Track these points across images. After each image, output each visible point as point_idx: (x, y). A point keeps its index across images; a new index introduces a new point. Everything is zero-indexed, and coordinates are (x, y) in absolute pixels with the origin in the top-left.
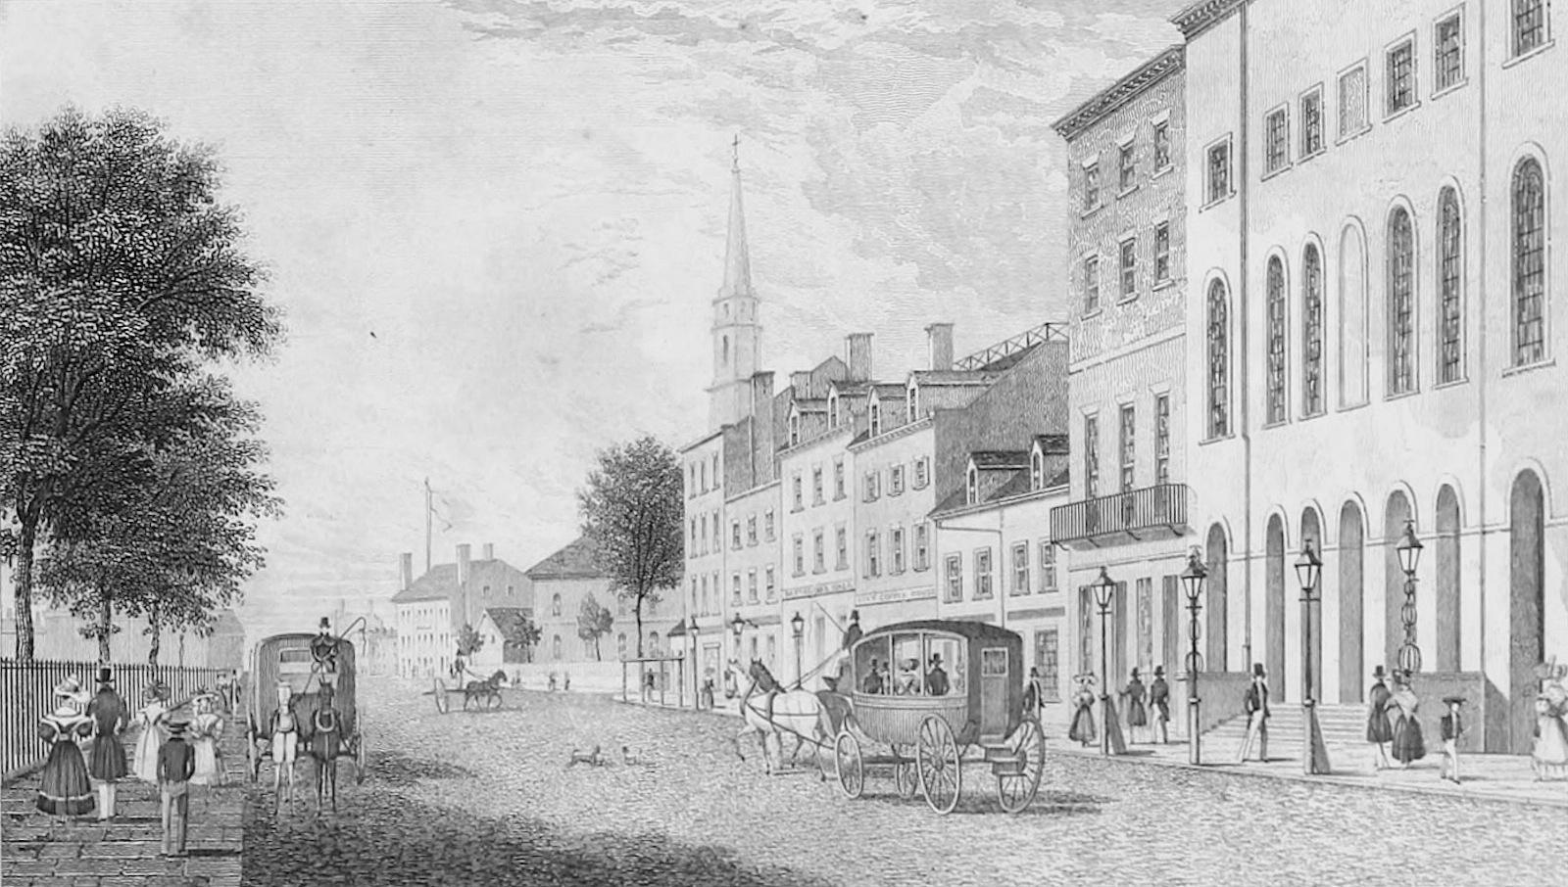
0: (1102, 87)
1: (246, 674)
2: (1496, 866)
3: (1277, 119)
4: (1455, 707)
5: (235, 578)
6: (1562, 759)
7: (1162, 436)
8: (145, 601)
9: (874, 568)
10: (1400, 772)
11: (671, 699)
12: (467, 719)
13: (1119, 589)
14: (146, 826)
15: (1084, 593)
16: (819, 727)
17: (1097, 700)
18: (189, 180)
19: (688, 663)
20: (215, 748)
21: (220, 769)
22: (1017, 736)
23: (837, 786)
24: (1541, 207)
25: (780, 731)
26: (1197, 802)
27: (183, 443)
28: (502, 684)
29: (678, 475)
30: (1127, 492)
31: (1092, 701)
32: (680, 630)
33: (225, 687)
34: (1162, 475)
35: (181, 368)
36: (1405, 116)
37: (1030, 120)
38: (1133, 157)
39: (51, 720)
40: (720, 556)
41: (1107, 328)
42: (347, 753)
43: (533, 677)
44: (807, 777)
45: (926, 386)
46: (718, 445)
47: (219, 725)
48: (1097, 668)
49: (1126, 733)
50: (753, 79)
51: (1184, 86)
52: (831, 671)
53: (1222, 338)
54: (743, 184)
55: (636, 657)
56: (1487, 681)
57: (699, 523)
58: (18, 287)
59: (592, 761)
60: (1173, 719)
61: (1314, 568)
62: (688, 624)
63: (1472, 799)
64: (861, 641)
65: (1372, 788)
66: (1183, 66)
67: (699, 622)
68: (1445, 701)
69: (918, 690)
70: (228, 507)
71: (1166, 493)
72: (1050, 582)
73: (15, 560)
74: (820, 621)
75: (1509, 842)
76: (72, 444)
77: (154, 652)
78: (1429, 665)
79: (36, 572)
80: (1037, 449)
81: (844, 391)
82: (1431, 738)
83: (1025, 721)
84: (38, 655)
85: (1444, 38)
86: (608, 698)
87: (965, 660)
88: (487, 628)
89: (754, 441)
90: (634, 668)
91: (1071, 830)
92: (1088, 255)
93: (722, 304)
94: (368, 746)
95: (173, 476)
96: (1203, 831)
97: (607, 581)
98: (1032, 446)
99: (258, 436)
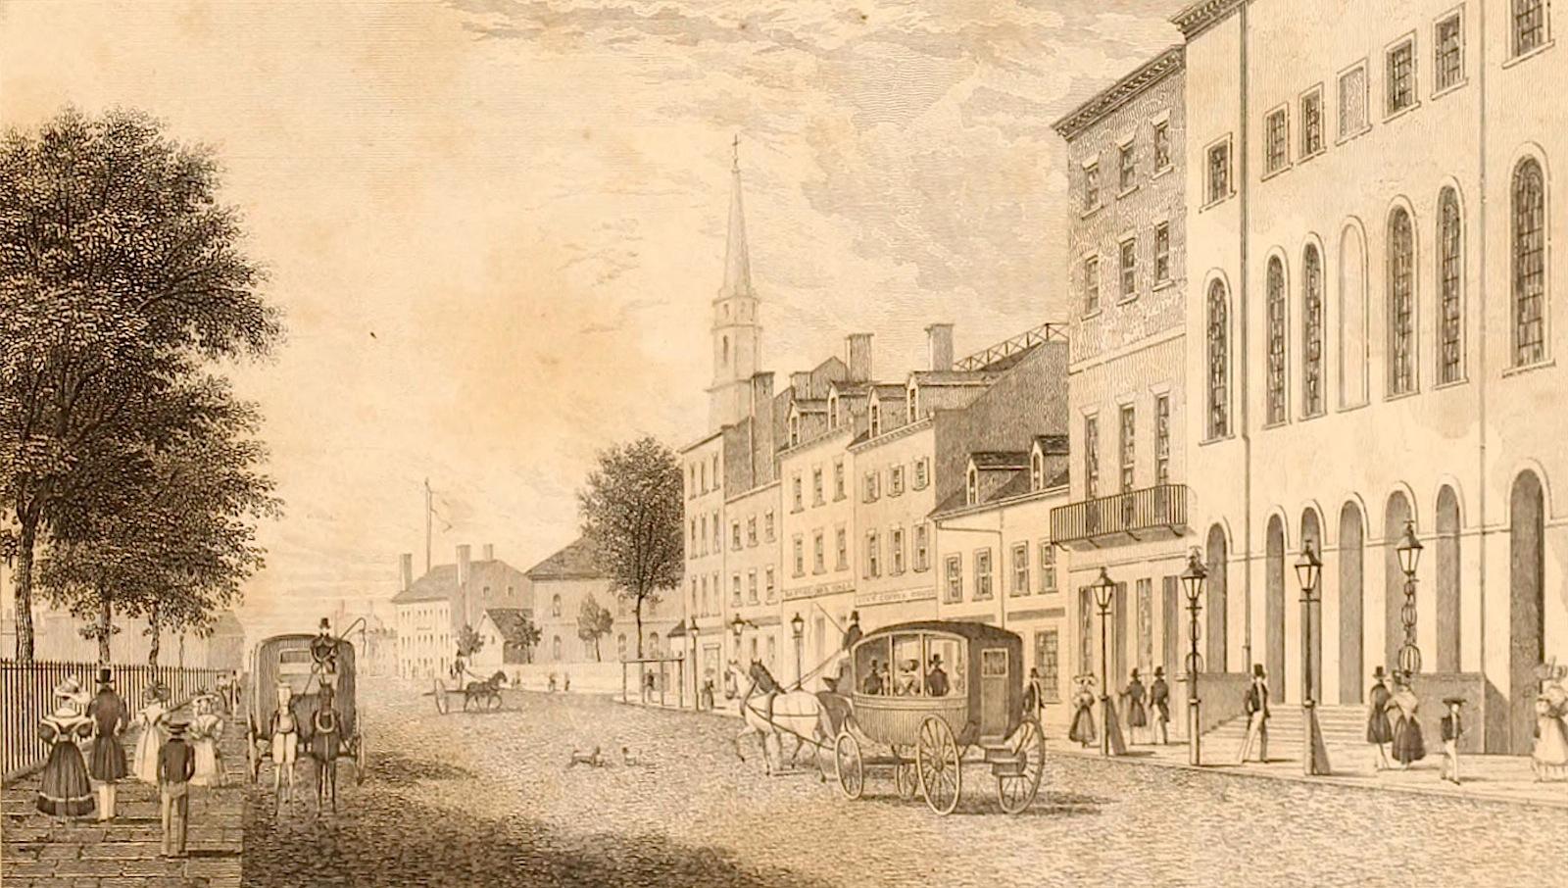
0: (1101, 87)
3: (1277, 119)
4: (1455, 707)
5: (235, 579)
6: (1562, 760)
7: (1162, 436)
8: (145, 602)
11: (672, 700)
12: (467, 720)
13: (1118, 589)
14: (146, 827)
15: (1084, 594)
16: (819, 727)
18: (189, 180)
19: (688, 664)
20: (215, 749)
21: (220, 770)
22: (1017, 737)
23: (837, 787)
24: (1541, 207)
26: (1197, 803)
28: (502, 685)
29: (678, 476)
30: (1127, 493)
31: (1092, 701)
32: (680, 631)
33: (225, 688)
35: (181, 369)
36: (1406, 116)
37: (1030, 120)
38: (1133, 158)
39: (51, 721)
42: (347, 754)
43: (533, 677)
44: (807, 778)
45: (926, 386)
46: (717, 445)
47: (219, 726)
48: (1097, 669)
49: (1126, 734)
50: (753, 79)
51: (1184, 86)
52: (831, 672)
54: (743, 184)
56: (1488, 682)
57: (699, 524)
58: (18, 287)
59: (592, 762)
61: (1314, 569)
62: (688, 625)
63: (1472, 800)
64: (861, 642)
65: (1372, 789)
66: (1183, 66)
67: (699, 623)
68: (1445, 702)
69: (918, 691)
70: (228, 507)
71: (1166, 494)
72: (1050, 582)
73: (15, 561)
74: (820, 622)
75: (1509, 843)
77: (154, 653)
78: (1429, 666)
79: (36, 573)
80: (1037, 449)
81: (844, 392)
82: (1431, 739)
83: (1025, 722)
84: (38, 656)
86: (608, 699)
87: (965, 661)
88: (487, 629)
89: (754, 442)
90: (634, 669)
92: (1088, 255)
93: (722, 305)
94: (368, 747)
96: (1203, 832)
97: (607, 582)
98: (1032, 447)
99: (258, 436)
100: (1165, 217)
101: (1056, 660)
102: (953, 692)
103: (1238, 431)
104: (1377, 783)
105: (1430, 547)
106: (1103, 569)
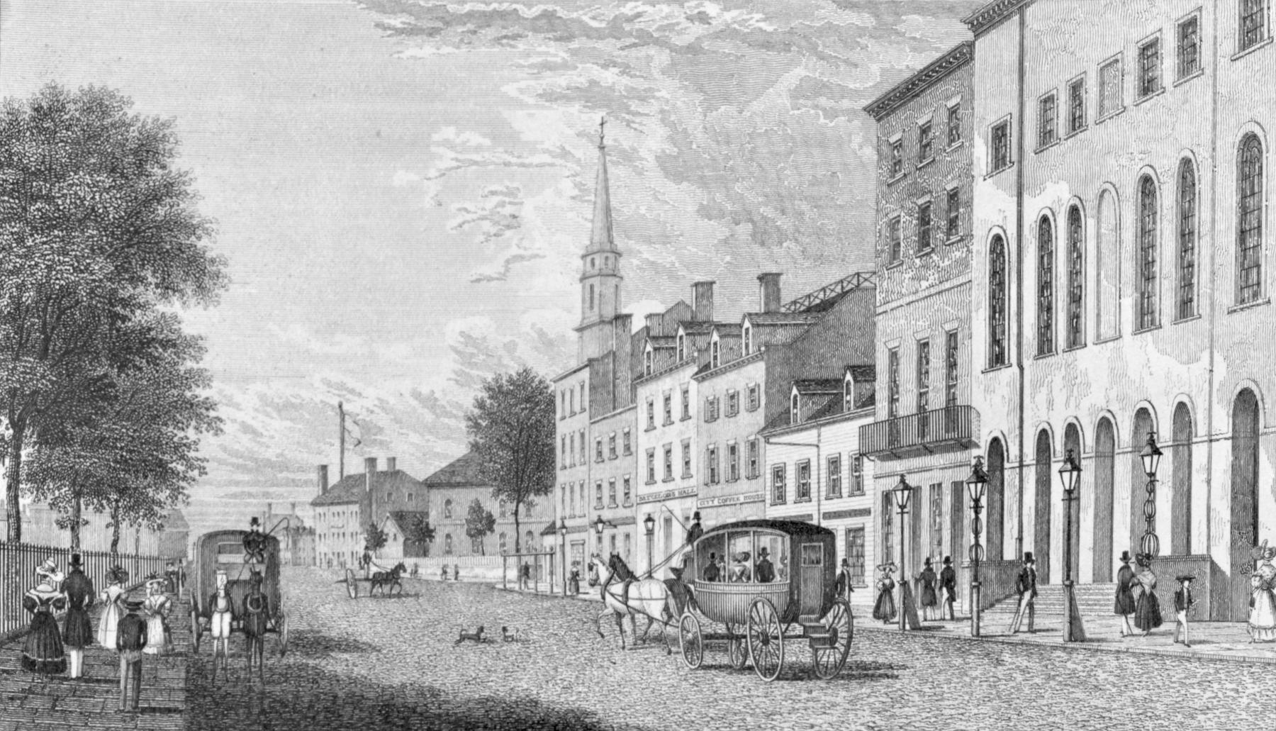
0: (907, 75)
1: (190, 563)
2: (1217, 712)
3: (1048, 101)
4: (1186, 583)
5: (182, 484)
6: (1271, 624)
7: (952, 365)
8: (108, 499)
9: (713, 476)
10: (1142, 639)
11: (544, 587)
12: (371, 604)
13: (915, 491)
14: (105, 686)
15: (887, 498)
16: (666, 609)
17: (897, 585)
18: (148, 148)
19: (558, 556)
20: (163, 623)
21: (168, 641)
22: (830, 615)
23: (681, 658)
24: (1260, 174)
25: (633, 612)
26: (977, 667)
27: (140, 369)
28: (402, 575)
29: (551, 402)
30: (923, 414)
31: (893, 585)
32: (551, 530)
33: (173, 573)
34: (951, 399)
35: (140, 306)
36: (1154, 101)
37: (846, 103)
38: (931, 135)
39: (33, 594)
40: (585, 468)
41: (907, 276)
42: (272, 630)
43: (429, 568)
44: (656, 651)
45: (758, 325)
46: (585, 374)
47: (168, 605)
48: (897, 561)
49: (920, 613)
50: (616, 70)
51: (973, 75)
52: (677, 562)
53: (1001, 284)
54: (608, 158)
55: (514, 552)
56: (1212, 563)
57: (568, 441)
58: (12, 233)
59: (477, 638)
60: (958, 600)
61: (1075, 474)
62: (558, 524)
63: (1199, 659)
64: (703, 538)
65: (1118, 652)
66: (972, 59)
67: (567, 523)
68: (1178, 579)
69: (749, 578)
70: (177, 424)
71: (955, 413)
72: (858, 488)
73: (7, 460)
74: (668, 521)
75: (1229, 693)
76: (52, 366)
77: (115, 543)
78: (1166, 549)
79: (24, 471)
80: (849, 377)
81: (690, 331)
82: (1166, 609)
83: (837, 603)
84: (25, 539)
85: (1185, 36)
86: (491, 587)
87: (788, 555)
88: (390, 528)
89: (615, 373)
90: (512, 561)
91: (872, 693)
92: (891, 216)
93: (589, 259)
94: (290, 626)
95: (132, 396)
96: (980, 691)
97: (491, 490)
98: (844, 375)
99: (201, 365)
100: (955, 184)
101: (863, 552)
102: (778, 578)
103: (1014, 360)
104: (1123, 647)
105: (1168, 454)
106: (902, 476)
